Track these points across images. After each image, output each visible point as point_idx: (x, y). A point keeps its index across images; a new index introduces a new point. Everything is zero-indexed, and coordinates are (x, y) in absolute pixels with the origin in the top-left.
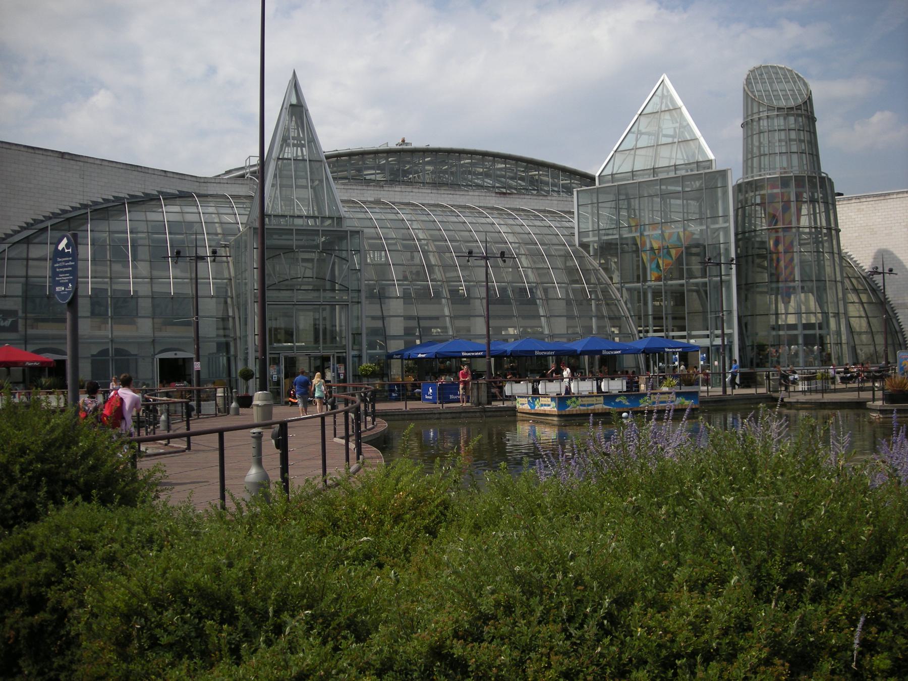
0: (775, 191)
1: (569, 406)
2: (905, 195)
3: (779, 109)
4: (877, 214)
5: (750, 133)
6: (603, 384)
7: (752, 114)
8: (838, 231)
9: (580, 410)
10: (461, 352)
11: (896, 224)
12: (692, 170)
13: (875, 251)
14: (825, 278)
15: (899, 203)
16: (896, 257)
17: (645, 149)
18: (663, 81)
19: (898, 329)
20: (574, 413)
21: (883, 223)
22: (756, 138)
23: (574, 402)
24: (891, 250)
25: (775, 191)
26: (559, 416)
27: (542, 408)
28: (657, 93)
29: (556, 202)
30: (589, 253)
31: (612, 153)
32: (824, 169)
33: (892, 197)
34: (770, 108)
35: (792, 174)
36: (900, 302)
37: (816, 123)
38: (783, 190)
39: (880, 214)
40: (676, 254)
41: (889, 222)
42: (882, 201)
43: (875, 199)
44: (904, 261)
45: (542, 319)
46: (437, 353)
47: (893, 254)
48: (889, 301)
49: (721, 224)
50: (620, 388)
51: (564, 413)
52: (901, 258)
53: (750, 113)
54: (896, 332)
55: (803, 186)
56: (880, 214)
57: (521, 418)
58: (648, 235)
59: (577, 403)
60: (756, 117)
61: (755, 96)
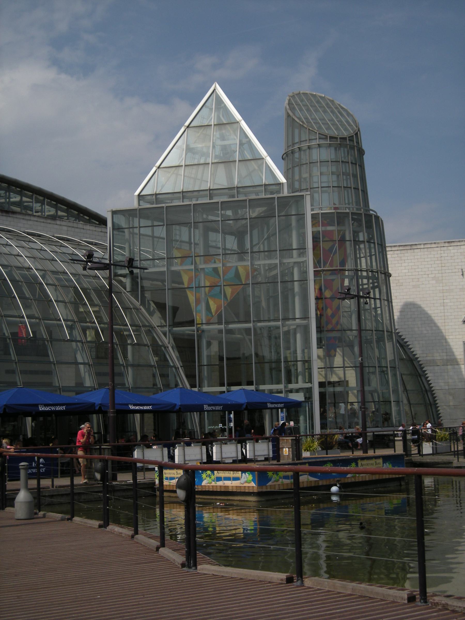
0: (329, 228)
1: (270, 480)
2: (463, 243)
3: (331, 138)
4: (403, 264)
5: (290, 166)
6: (176, 451)
7: (294, 144)
8: (388, 275)
9: (283, 484)
10: (37, 405)
11: (424, 276)
12: (257, 194)
13: (402, 304)
14: (383, 327)
15: (426, 253)
16: (424, 311)
17: (174, 169)
18: (214, 90)
19: (427, 387)
20: (277, 489)
21: (410, 274)
22: (297, 169)
23: (209, 476)
24: (419, 303)
25: (329, 228)
26: (259, 494)
27: (220, 483)
28: (207, 104)
29: (65, 228)
30: (125, 289)
31: (154, 169)
32: (371, 207)
33: (419, 247)
34: (323, 137)
35: (347, 211)
36: (428, 358)
37: (364, 156)
38: (339, 228)
39: (406, 264)
40: (232, 293)
41: (417, 274)
42: (409, 251)
43: (401, 248)
44: (432, 315)
45: (81, 367)
46: (6, 406)
47: (420, 307)
48: (417, 358)
49: (295, 258)
50: (234, 455)
51: (264, 490)
52: (429, 312)
53: (290, 143)
54: (426, 391)
55: (360, 225)
56: (406, 264)
57: (200, 500)
58: (203, 269)
59: (213, 477)
60: (296, 146)
61: (303, 122)
